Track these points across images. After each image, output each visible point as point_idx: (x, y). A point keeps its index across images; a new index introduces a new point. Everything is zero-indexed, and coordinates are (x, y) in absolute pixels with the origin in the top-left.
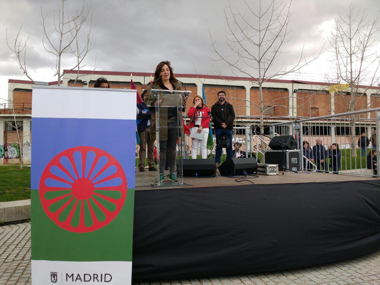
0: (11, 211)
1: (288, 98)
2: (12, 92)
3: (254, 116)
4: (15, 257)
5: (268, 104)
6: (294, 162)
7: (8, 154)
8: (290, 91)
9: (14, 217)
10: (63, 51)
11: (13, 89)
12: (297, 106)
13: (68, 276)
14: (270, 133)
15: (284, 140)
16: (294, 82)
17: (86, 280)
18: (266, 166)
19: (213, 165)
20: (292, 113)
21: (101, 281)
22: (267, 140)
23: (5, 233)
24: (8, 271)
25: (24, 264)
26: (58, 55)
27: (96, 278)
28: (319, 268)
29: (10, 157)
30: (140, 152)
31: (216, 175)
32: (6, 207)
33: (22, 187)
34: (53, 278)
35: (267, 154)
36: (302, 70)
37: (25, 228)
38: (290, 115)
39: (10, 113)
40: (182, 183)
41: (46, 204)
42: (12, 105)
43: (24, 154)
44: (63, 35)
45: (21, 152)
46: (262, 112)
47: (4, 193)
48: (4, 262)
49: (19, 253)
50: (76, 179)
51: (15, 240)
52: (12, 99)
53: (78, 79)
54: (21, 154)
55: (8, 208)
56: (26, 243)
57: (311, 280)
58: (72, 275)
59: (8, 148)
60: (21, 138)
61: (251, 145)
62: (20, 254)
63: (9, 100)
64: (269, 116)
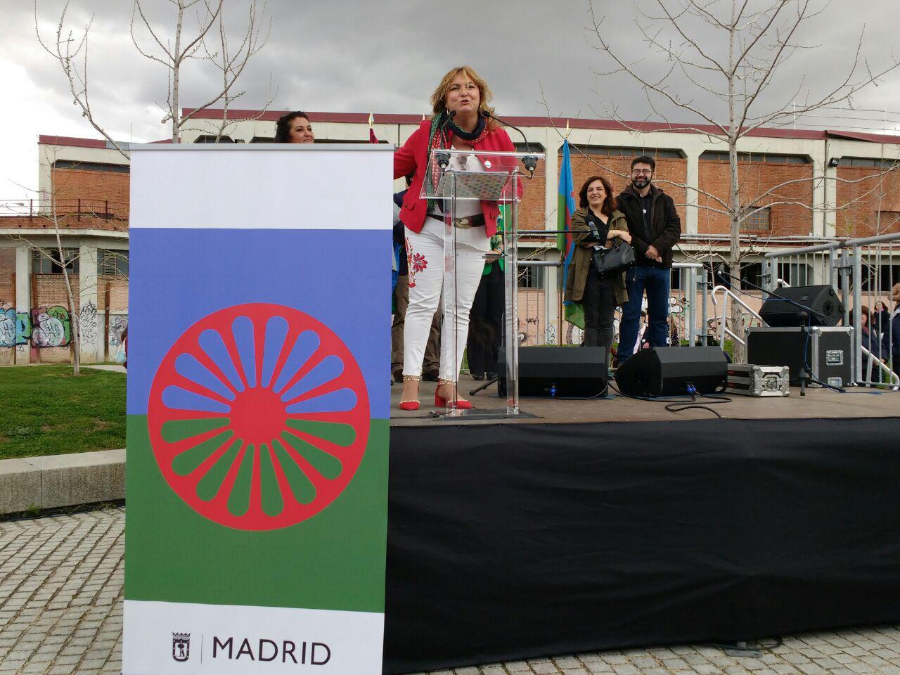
1: (812, 180)
2: (49, 169)
3: (711, 235)
4: (75, 597)
5: (751, 202)
6: (835, 362)
7: (42, 335)
10: (186, 54)
11: (52, 161)
12: (838, 205)
13: (218, 644)
14: (764, 280)
16: (828, 136)
17: (263, 657)
18: (753, 371)
19: (601, 365)
20: (823, 227)
21: (303, 662)
22: (752, 304)
23: (43, 537)
25: (98, 613)
26: (173, 64)
27: (290, 652)
29: (45, 344)
30: (395, 329)
31: (606, 392)
32: (45, 468)
33: (85, 419)
34: (178, 650)
36: (857, 100)
37: (96, 525)
38: (817, 233)
39: (44, 226)
40: (516, 412)
41: (165, 453)
42: (49, 203)
44: (184, 11)
45: (75, 330)
46: (736, 220)
47: (38, 434)
48: (46, 608)
49: (83, 586)
50: (241, 389)
51: (70, 555)
52: (49, 189)
53: (224, 133)
54: (76, 335)
55: (50, 471)
56: (100, 562)
58: (230, 640)
59: (40, 319)
60: (76, 291)
61: (708, 314)
62: (84, 589)
63: (42, 191)
64: (755, 236)
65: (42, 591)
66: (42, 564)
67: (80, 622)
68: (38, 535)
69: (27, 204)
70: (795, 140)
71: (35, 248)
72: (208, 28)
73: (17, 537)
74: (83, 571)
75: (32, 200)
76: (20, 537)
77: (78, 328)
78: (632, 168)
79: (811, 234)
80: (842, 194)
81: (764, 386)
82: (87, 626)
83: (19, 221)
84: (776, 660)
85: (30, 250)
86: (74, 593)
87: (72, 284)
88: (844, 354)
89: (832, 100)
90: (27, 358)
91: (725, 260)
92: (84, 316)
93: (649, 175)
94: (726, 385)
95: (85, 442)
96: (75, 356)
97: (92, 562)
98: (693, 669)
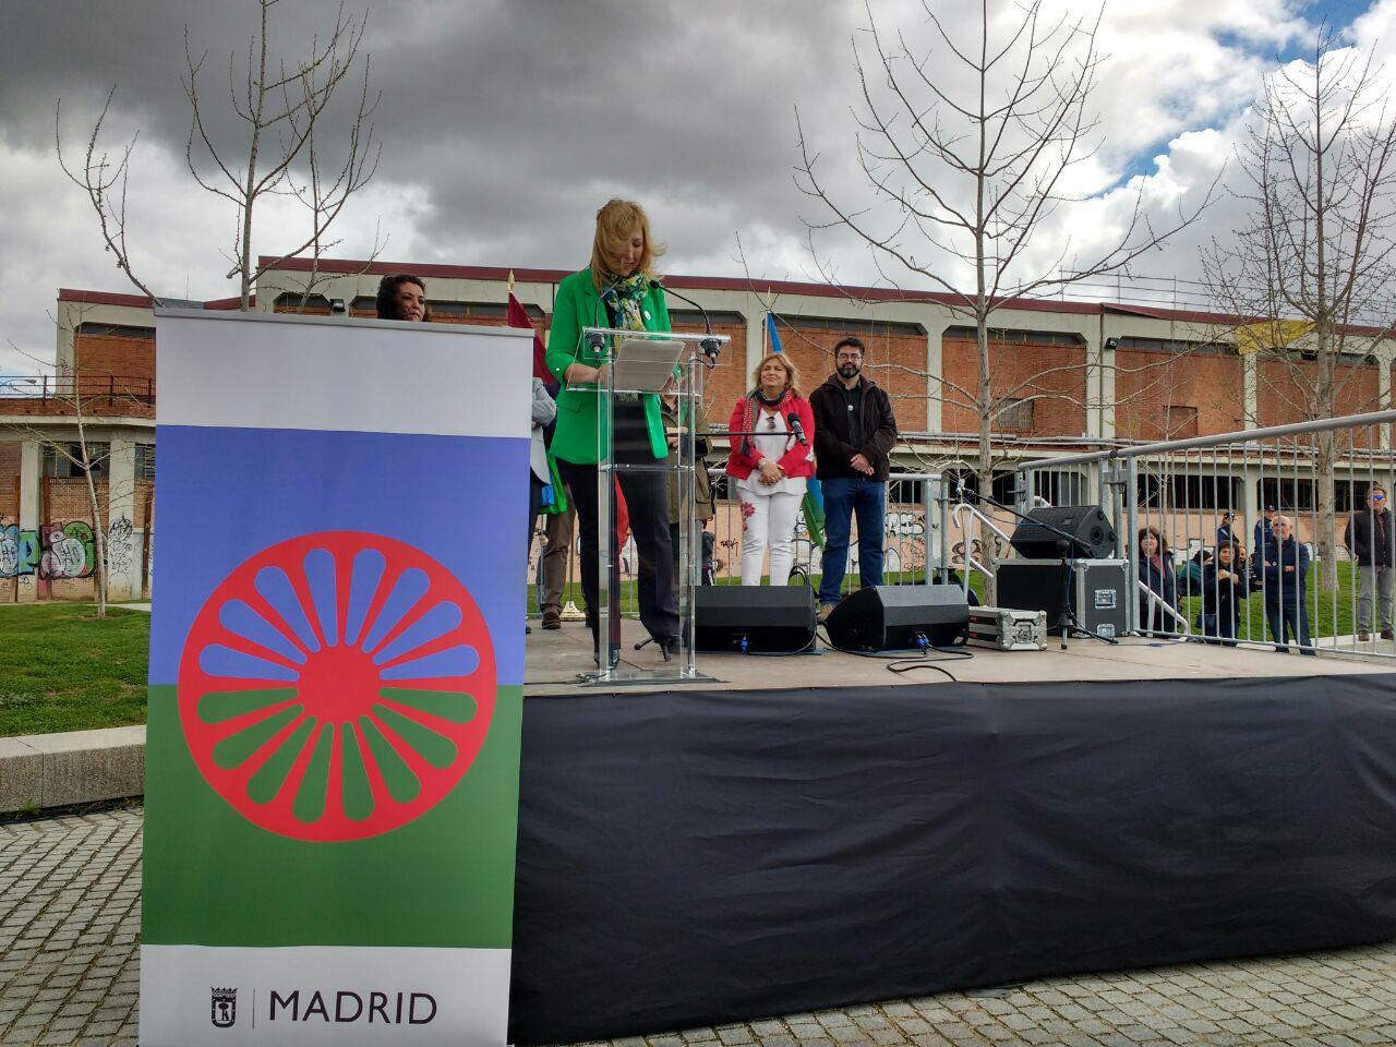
2: (71, 335)
4: (82, 932)
5: (1011, 391)
7: (55, 560)
8: (1093, 345)
10: (262, 188)
11: (77, 323)
14: (1018, 498)
20: (1100, 426)
21: (398, 1021)
22: (1004, 524)
23: (44, 848)
25: (113, 957)
26: (244, 201)
27: (380, 1008)
29: (58, 574)
32: (47, 751)
33: (107, 681)
34: (219, 1012)
35: (1005, 573)
37: (117, 831)
38: (1092, 433)
40: (692, 674)
41: (202, 738)
42: (70, 381)
43: (110, 564)
46: (986, 417)
48: (41, 949)
49: (95, 917)
52: (70, 361)
55: (54, 754)
56: (121, 883)
58: (295, 995)
59: (53, 540)
60: (104, 502)
62: (96, 922)
63: (61, 365)
64: (1014, 436)
65: (37, 924)
66: (39, 886)
67: (88, 969)
68: (35, 846)
69: (40, 382)
70: (1064, 315)
71: (48, 442)
72: (294, 154)
73: (6, 847)
74: (96, 895)
75: (46, 377)
76: (11, 848)
77: (105, 552)
78: (836, 353)
79: (1084, 434)
80: (1123, 384)
82: (98, 975)
83: (27, 405)
84: (1029, 1001)
85: (41, 446)
86: (83, 926)
87: (99, 491)
88: (1117, 593)
89: (1365, 166)
90: (33, 593)
91: (971, 467)
92: (114, 536)
93: (858, 362)
94: (967, 635)
95: (106, 713)
96: (100, 591)
97: (108, 883)
98: (921, 1017)
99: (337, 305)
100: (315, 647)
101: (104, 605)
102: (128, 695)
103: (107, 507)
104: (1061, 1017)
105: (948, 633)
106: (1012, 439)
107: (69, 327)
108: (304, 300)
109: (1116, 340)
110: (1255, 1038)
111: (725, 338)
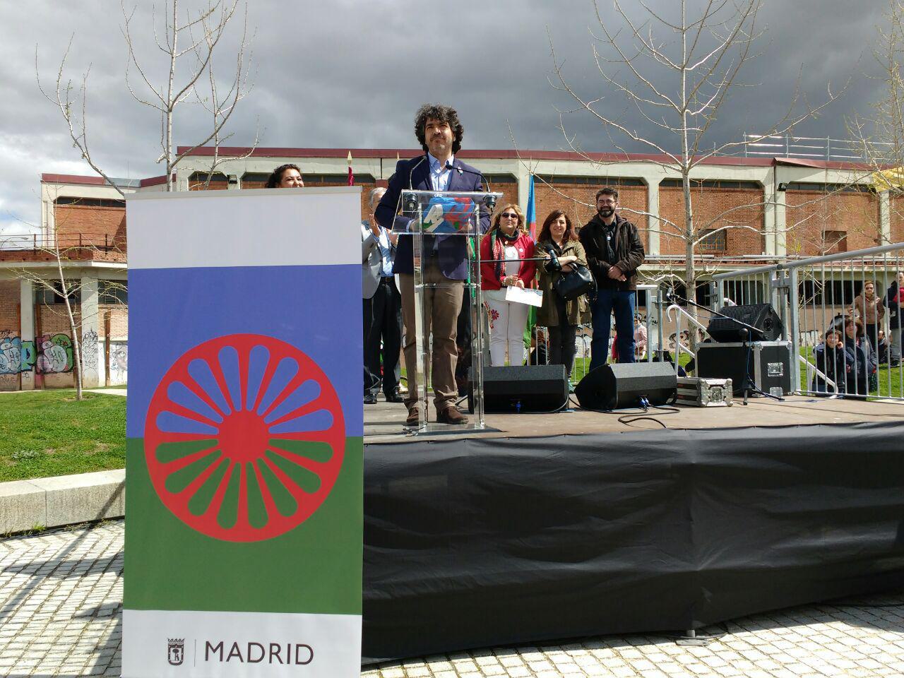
0: (61, 499)
7: (46, 361)
8: (769, 190)
9: (70, 515)
11: (54, 198)
14: (711, 300)
15: (747, 316)
17: (251, 659)
20: (776, 248)
21: (289, 662)
22: (700, 320)
24: (61, 640)
28: (819, 610)
29: (49, 370)
32: (49, 489)
34: (173, 655)
35: (702, 353)
38: (770, 253)
43: (84, 362)
57: (817, 672)
58: (221, 644)
59: (44, 347)
62: (86, 602)
64: (712, 256)
73: (24, 554)
79: (763, 253)
80: (792, 216)
81: (710, 397)
84: (724, 647)
93: (613, 205)
94: (676, 397)
98: (647, 658)
99: (232, 179)
100: (238, 408)
101: (81, 391)
102: (102, 450)
103: (80, 324)
104: (745, 658)
105: (663, 394)
106: (711, 258)
107: (49, 201)
108: (209, 178)
109: (786, 185)
110: (882, 672)
111: (500, 194)
